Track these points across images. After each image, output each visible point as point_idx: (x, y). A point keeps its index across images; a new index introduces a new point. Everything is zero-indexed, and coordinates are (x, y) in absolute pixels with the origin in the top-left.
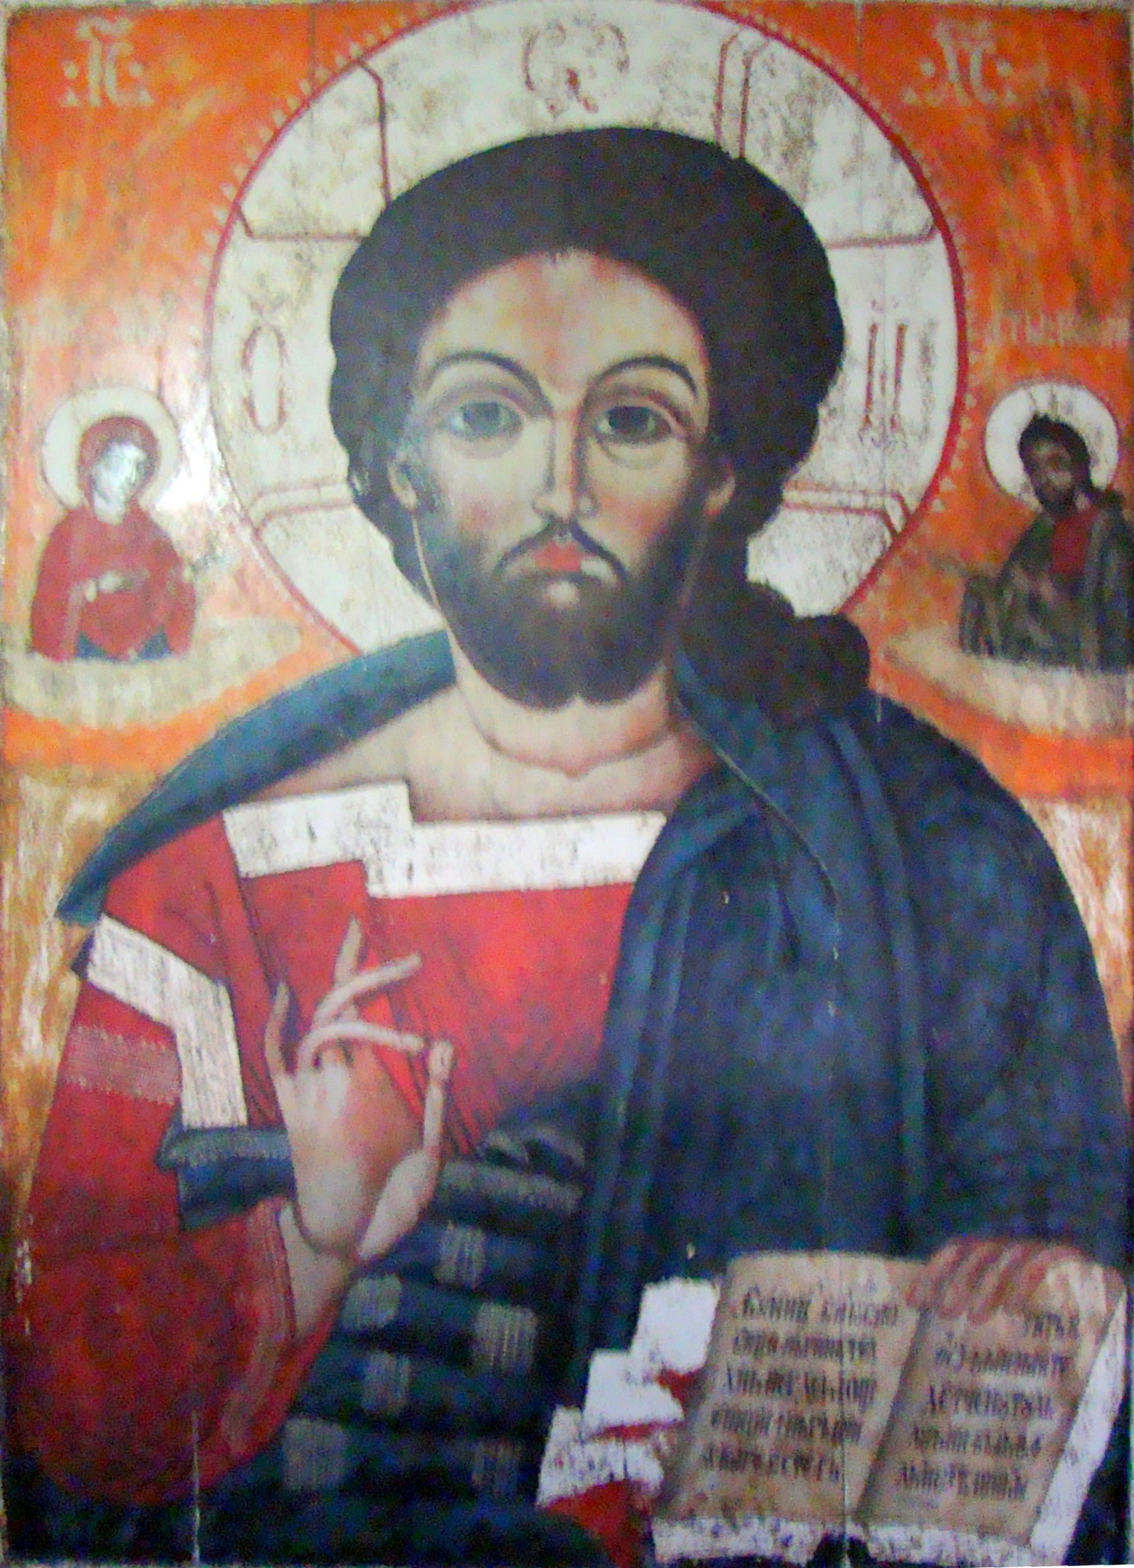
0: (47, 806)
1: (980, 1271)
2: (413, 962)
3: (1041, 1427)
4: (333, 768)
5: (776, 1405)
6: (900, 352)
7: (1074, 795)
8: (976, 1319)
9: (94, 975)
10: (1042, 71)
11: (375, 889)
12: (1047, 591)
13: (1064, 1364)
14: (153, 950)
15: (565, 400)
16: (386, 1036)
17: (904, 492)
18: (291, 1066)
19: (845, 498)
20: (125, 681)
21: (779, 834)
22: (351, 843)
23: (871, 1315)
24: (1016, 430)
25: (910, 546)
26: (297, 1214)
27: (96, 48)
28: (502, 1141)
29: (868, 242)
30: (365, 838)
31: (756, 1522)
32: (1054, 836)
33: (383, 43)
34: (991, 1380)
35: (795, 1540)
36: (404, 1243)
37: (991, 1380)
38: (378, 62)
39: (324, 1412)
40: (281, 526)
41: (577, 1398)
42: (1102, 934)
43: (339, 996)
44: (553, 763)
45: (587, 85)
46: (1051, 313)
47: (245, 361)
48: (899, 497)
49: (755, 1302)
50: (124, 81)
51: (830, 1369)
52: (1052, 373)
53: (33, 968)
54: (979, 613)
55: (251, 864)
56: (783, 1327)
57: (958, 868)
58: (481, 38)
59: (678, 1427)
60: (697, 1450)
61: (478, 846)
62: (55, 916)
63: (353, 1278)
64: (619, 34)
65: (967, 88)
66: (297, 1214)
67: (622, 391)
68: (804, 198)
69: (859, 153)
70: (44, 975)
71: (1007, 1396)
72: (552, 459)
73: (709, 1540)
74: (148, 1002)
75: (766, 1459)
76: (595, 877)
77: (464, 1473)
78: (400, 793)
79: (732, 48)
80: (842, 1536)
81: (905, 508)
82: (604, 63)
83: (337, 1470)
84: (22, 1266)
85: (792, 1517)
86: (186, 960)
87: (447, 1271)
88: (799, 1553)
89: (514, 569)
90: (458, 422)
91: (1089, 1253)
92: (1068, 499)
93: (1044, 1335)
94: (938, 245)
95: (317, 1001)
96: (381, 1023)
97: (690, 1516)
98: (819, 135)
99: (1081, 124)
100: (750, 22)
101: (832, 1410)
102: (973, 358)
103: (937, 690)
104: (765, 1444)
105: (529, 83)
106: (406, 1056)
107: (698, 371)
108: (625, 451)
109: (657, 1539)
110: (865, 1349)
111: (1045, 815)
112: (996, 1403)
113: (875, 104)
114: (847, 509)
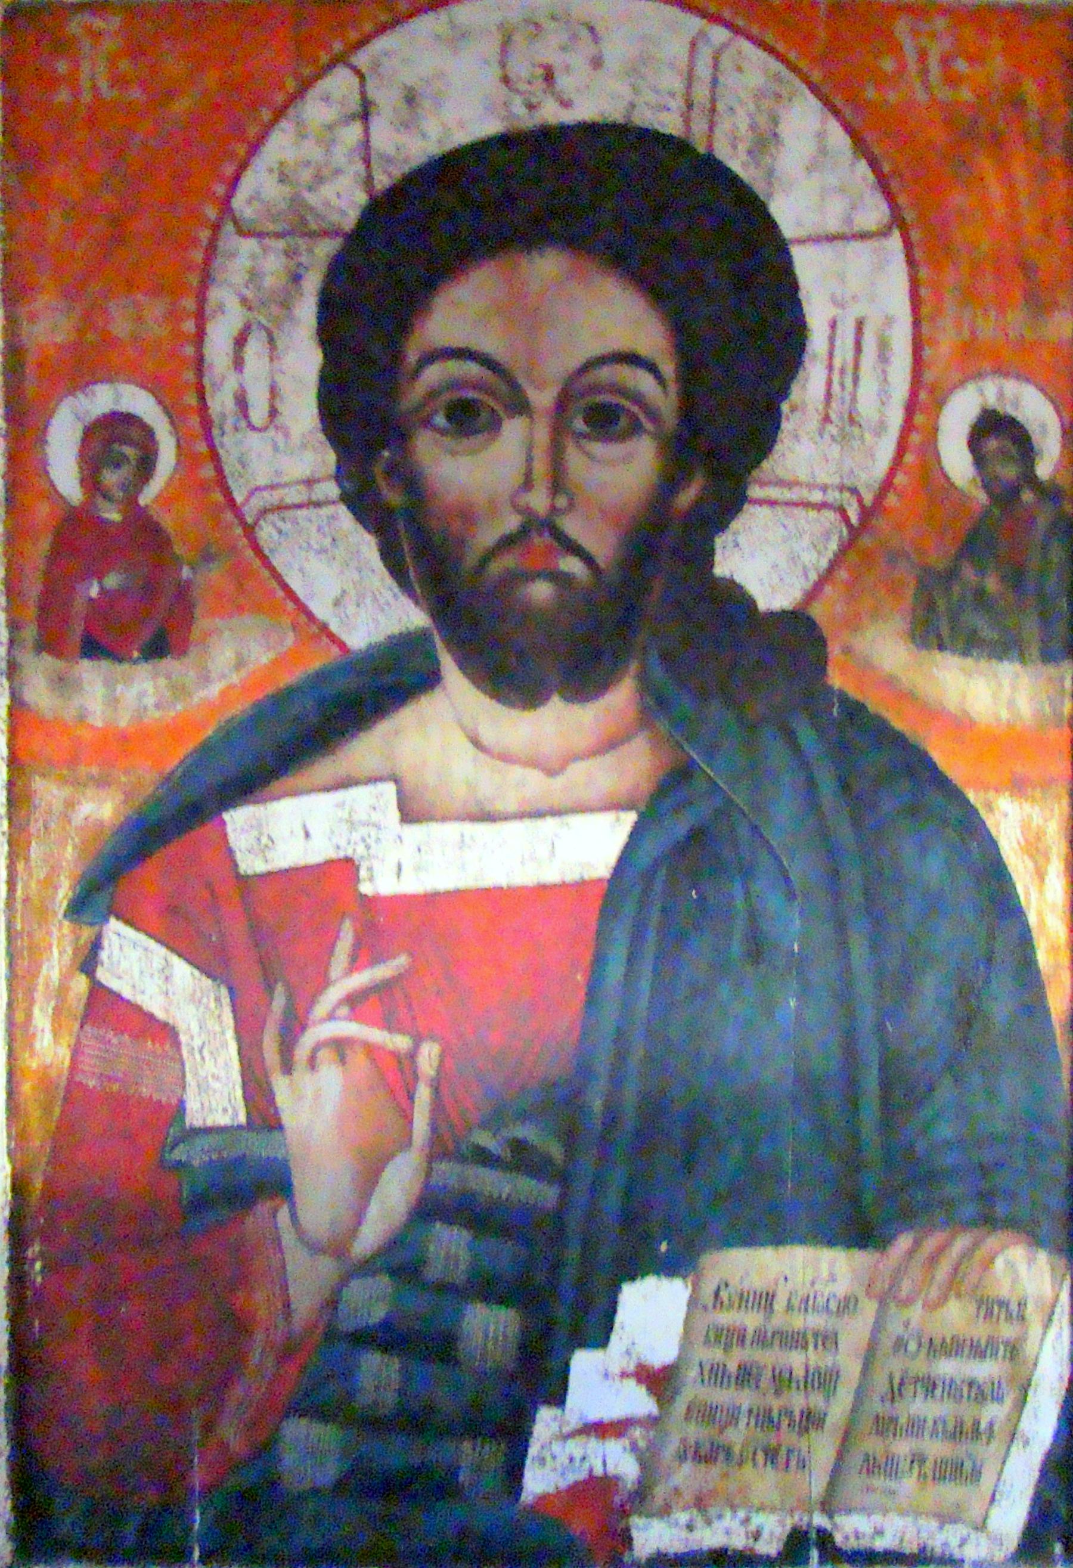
0: (58, 806)
1: (933, 1260)
2: (402, 960)
3: (994, 1412)
4: (325, 768)
5: (746, 1399)
6: (858, 348)
7: (1019, 787)
8: (931, 1307)
9: (103, 975)
10: (997, 65)
11: (366, 888)
12: (992, 585)
13: (1014, 1350)
14: (159, 952)
15: (543, 398)
16: (377, 1035)
17: (863, 491)
18: (287, 1068)
19: (805, 494)
20: (128, 681)
21: (743, 832)
22: (343, 843)
23: (833, 1306)
24: (967, 426)
25: (866, 541)
26: (294, 1216)
27: (87, 43)
28: (484, 1139)
29: (831, 238)
30: (356, 836)
31: (728, 1514)
32: (997, 825)
33: (364, 41)
34: (946, 1368)
35: (765, 1535)
36: (393, 1244)
37: (946, 1368)
38: (361, 59)
39: (321, 1414)
40: (274, 525)
41: (559, 1399)
42: (1041, 922)
43: (334, 994)
44: (533, 763)
45: (564, 82)
46: (1002, 311)
47: (238, 364)
48: (854, 491)
49: (724, 1294)
50: (118, 81)
51: (796, 1360)
52: (1001, 370)
53: (44, 970)
54: (930, 606)
55: (250, 864)
56: (752, 1320)
57: (909, 853)
58: (459, 37)
59: (652, 1422)
60: (670, 1450)
61: (462, 843)
62: (65, 916)
63: (343, 1282)
64: (592, 29)
65: (926, 85)
66: (294, 1216)
67: (596, 389)
68: (770, 195)
69: (823, 150)
70: (55, 975)
71: (963, 1382)
72: (529, 460)
73: (684, 1534)
74: (153, 1002)
75: (737, 1449)
76: (572, 876)
77: (453, 1471)
78: (389, 790)
79: (700, 45)
80: (809, 1525)
81: (860, 500)
82: (578, 61)
83: (331, 1470)
84: (32, 1265)
85: (762, 1508)
86: (190, 961)
87: (434, 1272)
88: (769, 1547)
89: (495, 568)
90: (440, 420)
91: (1035, 1240)
92: (1014, 491)
93: (994, 1320)
94: (895, 242)
95: (312, 1003)
96: (373, 1023)
97: (665, 1511)
98: (783, 129)
99: (1033, 118)
100: (716, 19)
101: (797, 1401)
102: (928, 352)
103: (889, 683)
104: (736, 1436)
105: (506, 80)
106: (395, 1054)
107: (668, 368)
108: (597, 448)
109: (635, 1533)
110: (828, 1340)
111: (989, 807)
112: (953, 1391)
113: (838, 101)
114: (806, 505)
